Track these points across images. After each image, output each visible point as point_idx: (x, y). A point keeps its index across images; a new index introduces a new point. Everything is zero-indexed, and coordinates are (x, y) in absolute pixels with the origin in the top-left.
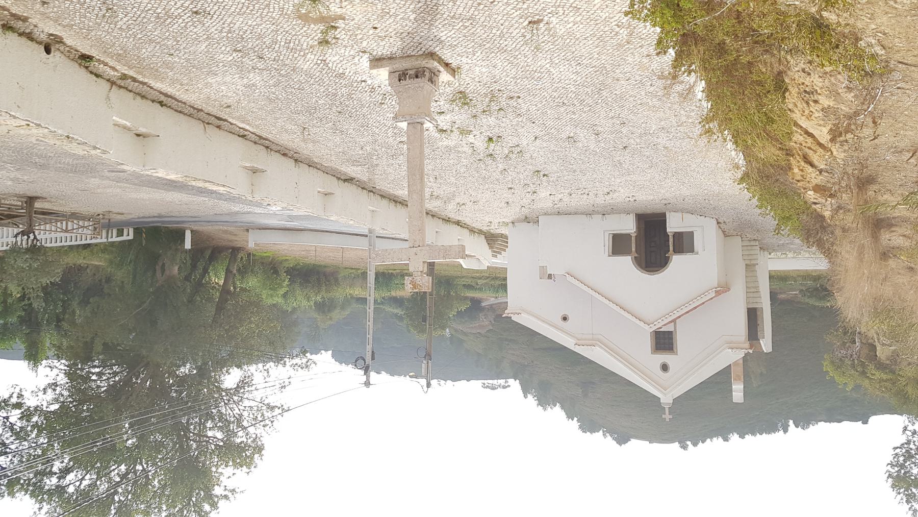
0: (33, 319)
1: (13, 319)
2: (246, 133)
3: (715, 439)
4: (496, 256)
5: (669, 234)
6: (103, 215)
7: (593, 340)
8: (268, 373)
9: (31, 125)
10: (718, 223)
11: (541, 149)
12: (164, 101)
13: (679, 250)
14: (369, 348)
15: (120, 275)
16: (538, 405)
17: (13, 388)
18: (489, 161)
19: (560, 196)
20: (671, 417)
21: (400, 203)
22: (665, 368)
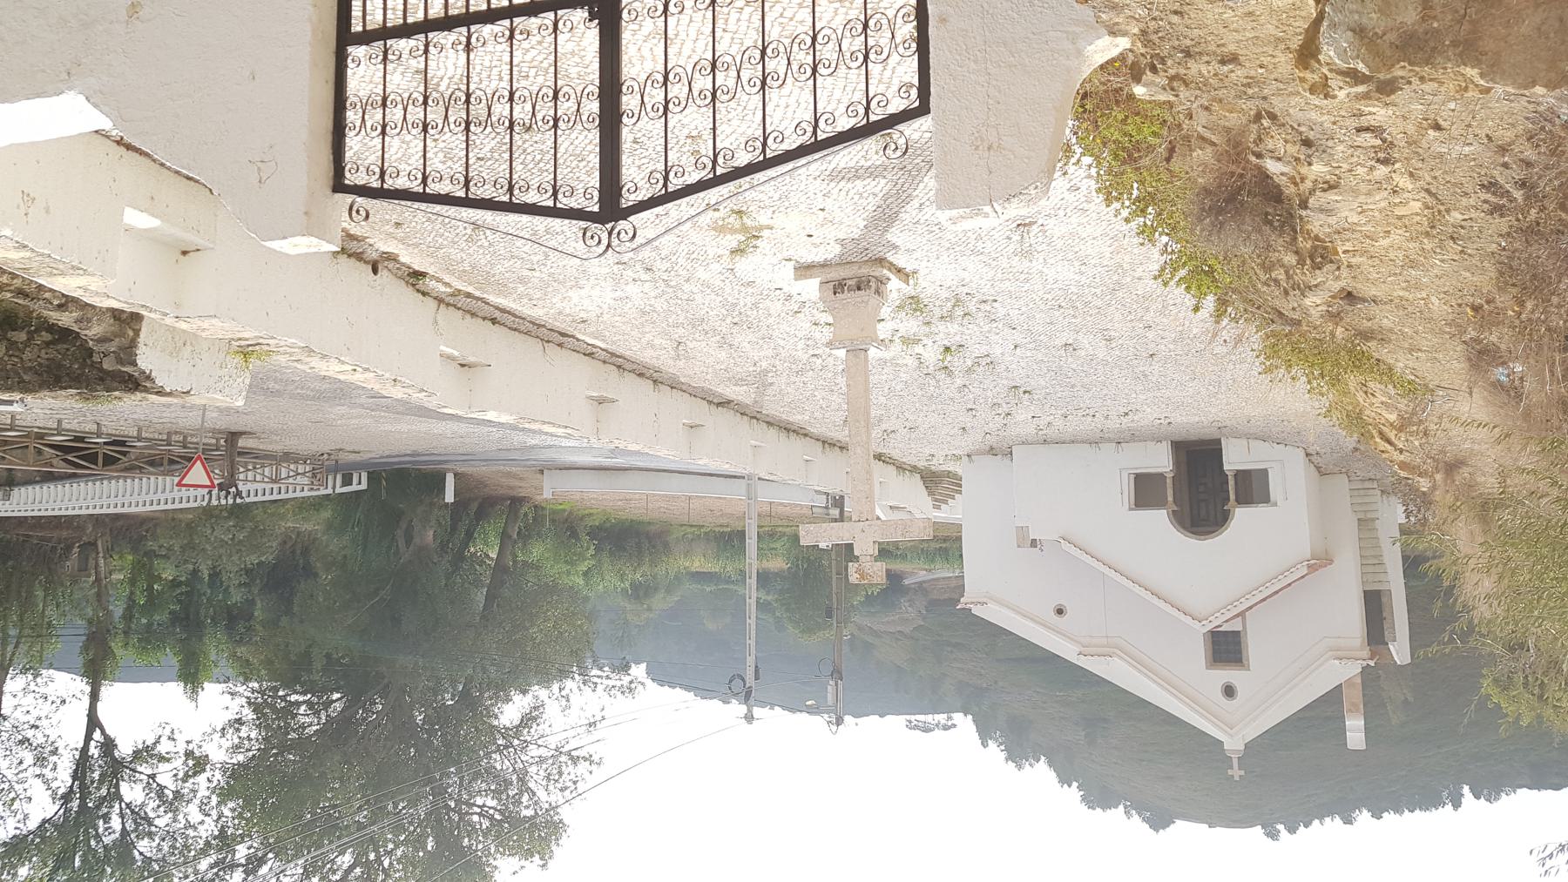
0: (191, 617)
1: (161, 617)
2: (594, 350)
3: (1328, 820)
4: (939, 508)
6: (329, 454)
8: (568, 701)
9: (358, 369)
10: (1307, 455)
11: (1022, 358)
12: (498, 318)
13: (1246, 498)
14: (751, 661)
15: (336, 545)
16: (1007, 760)
17: (161, 729)
18: (942, 376)
19: (1048, 419)
20: (1242, 773)
21: (794, 431)
22: (1229, 691)
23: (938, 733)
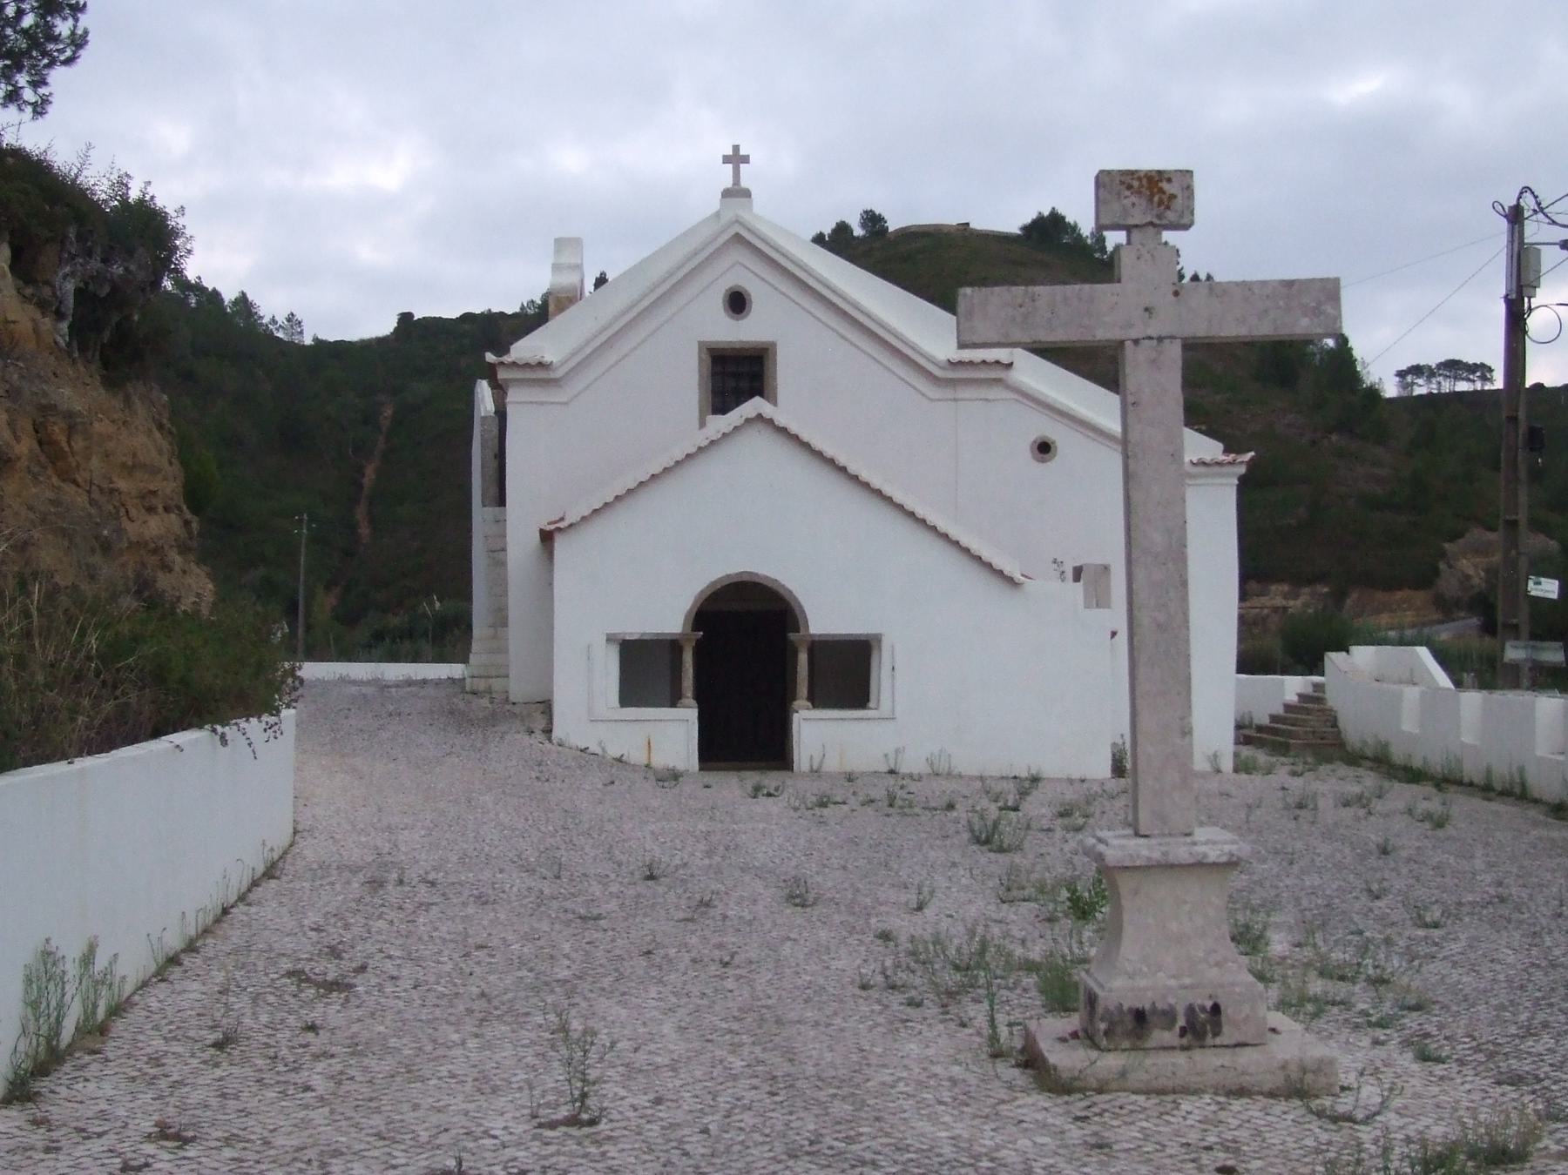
5: (694, 703)
22: (737, 303)
23: (1433, 361)
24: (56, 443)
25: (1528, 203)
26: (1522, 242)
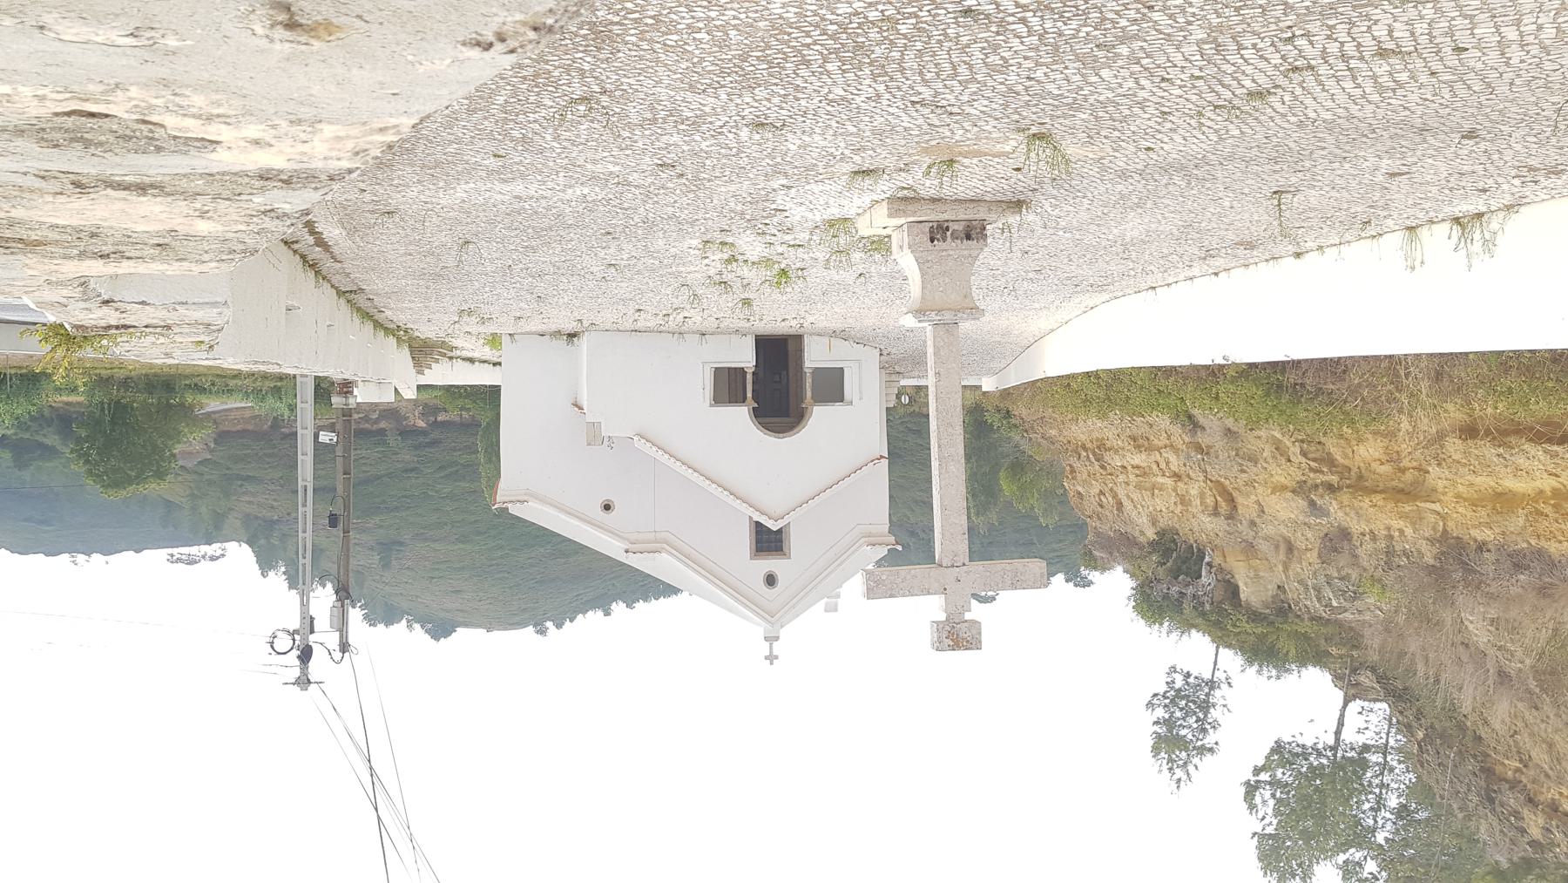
7: (656, 541)
22: (771, 580)
23: (205, 565)
24: (1225, 501)
25: (337, 655)
26: (341, 631)
